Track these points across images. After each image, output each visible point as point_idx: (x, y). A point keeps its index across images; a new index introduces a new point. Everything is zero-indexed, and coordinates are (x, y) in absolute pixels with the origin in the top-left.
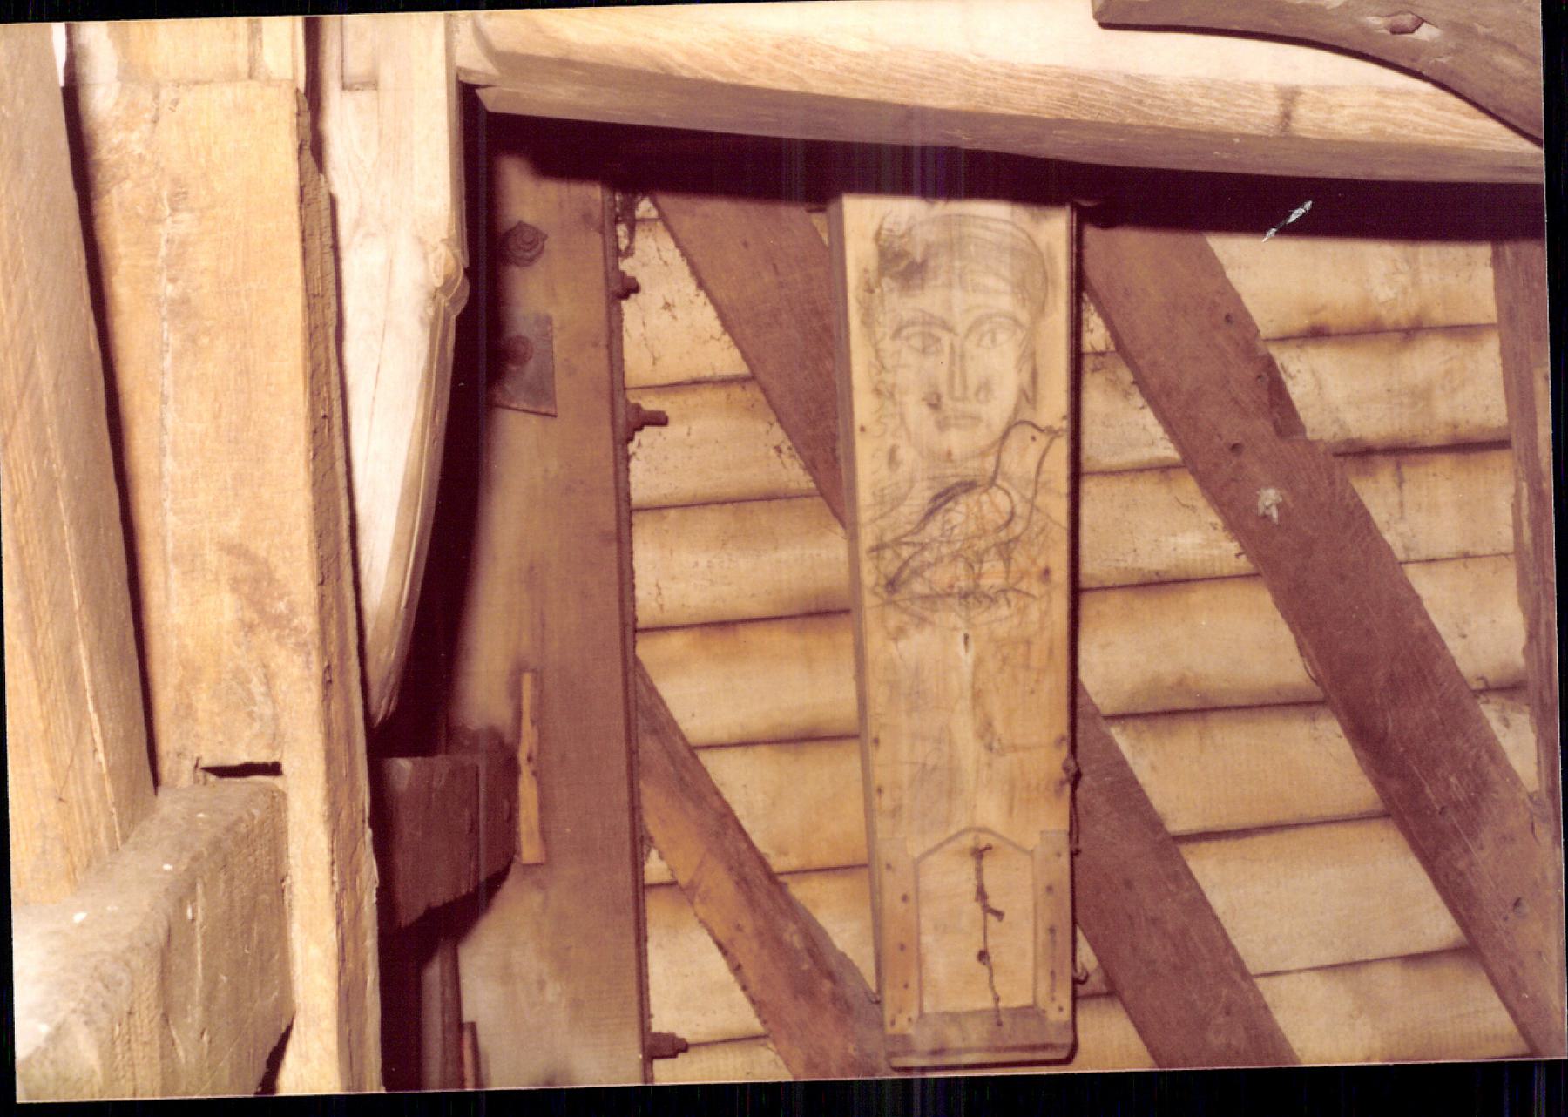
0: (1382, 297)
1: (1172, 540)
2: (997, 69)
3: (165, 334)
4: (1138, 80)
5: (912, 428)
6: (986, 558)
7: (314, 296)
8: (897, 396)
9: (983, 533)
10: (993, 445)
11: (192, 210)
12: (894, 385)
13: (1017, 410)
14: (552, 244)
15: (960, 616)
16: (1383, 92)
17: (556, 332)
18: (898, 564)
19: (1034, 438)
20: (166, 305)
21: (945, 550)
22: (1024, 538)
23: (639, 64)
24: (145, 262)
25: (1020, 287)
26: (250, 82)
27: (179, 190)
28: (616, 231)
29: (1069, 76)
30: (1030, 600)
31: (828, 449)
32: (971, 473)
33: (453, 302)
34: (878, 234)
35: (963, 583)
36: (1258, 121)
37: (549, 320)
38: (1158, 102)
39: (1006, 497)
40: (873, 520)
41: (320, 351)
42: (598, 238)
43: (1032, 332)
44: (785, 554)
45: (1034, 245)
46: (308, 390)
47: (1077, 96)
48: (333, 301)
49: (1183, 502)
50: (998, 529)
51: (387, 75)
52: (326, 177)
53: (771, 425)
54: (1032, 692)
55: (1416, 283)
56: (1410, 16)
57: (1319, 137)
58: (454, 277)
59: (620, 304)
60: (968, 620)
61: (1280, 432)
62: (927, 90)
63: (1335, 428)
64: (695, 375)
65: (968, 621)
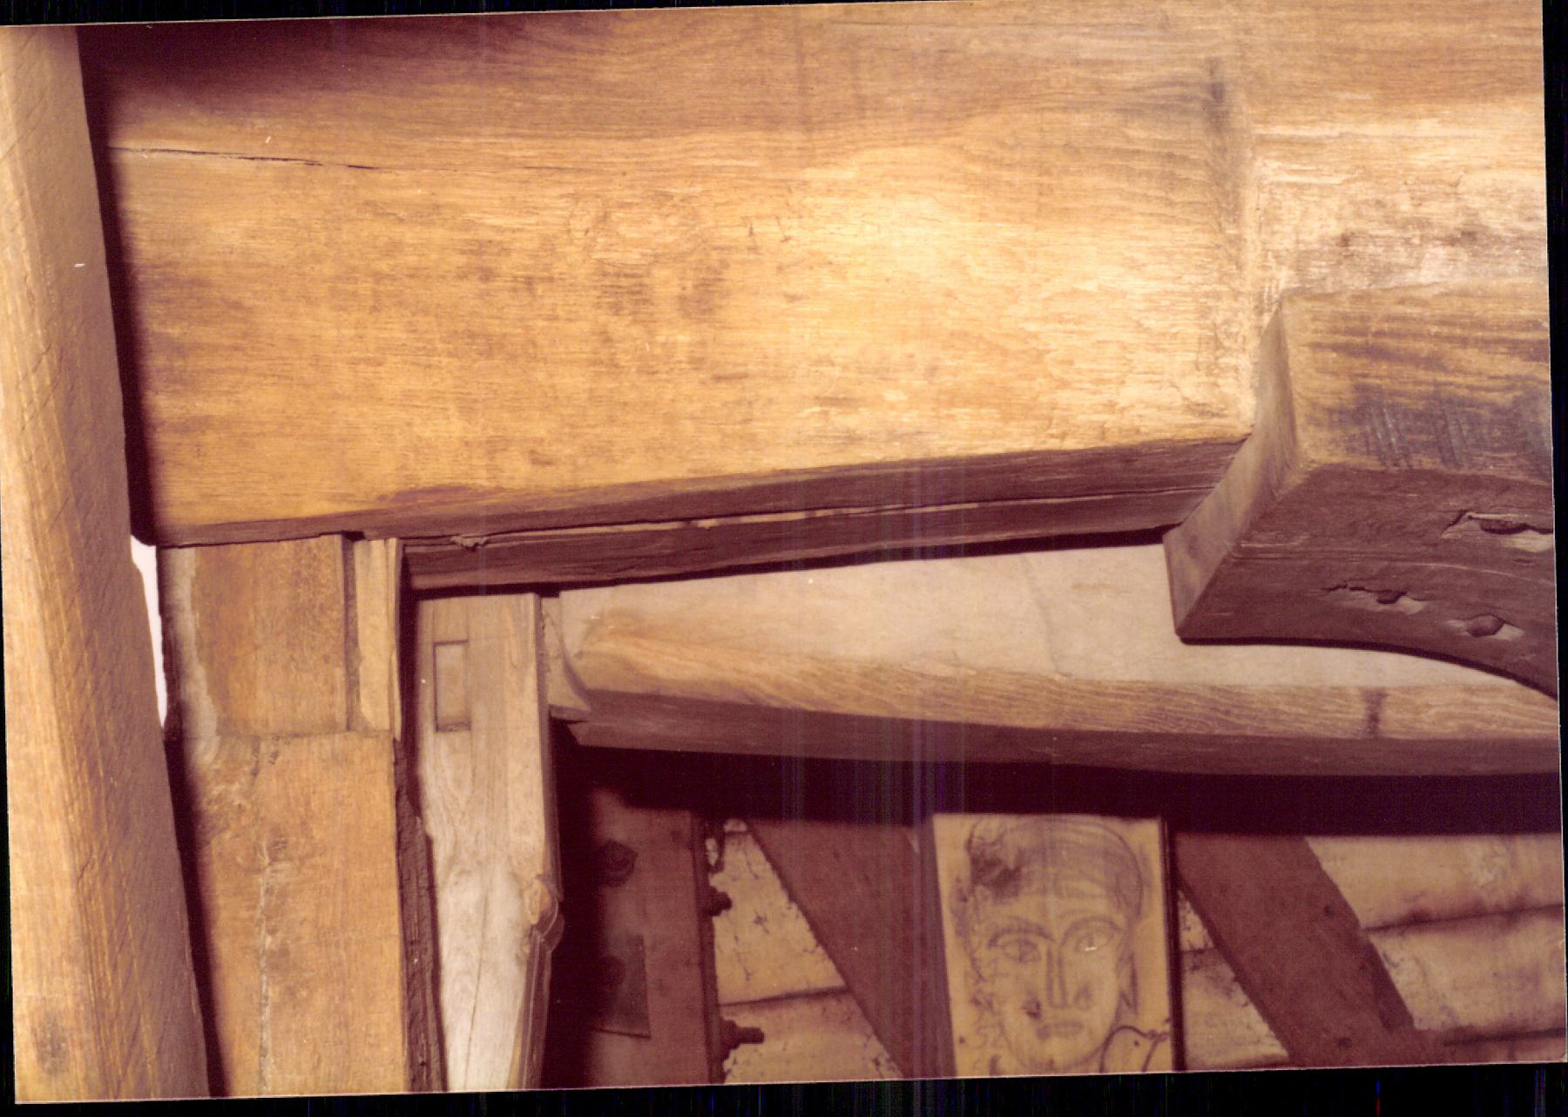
0: (1482, 881)
2: (1083, 687)
3: (264, 987)
4: (1226, 691)
7: (412, 943)
8: (996, 1005)
10: (1093, 1055)
11: (290, 859)
12: (992, 995)
13: (1118, 1014)
14: (641, 863)
16: (1469, 690)
17: (648, 953)
20: (265, 958)
23: (730, 697)
24: (244, 914)
25: (1116, 891)
26: (347, 734)
27: (278, 839)
29: (1154, 690)
33: (548, 939)
34: (970, 841)
36: (1347, 725)
37: (640, 940)
38: (1246, 712)
41: (418, 998)
42: (685, 855)
45: (1126, 847)
46: (406, 1040)
47: (1164, 710)
48: (429, 946)
51: (480, 714)
52: (422, 818)
55: (1514, 865)
56: (1491, 618)
57: (1409, 737)
58: (550, 913)
59: (711, 920)
61: (1388, 1025)
62: (1015, 710)
63: (1444, 1017)
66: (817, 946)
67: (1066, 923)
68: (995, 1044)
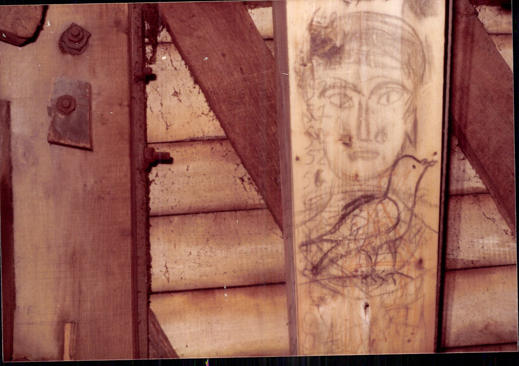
1: (481, 241)
5: (332, 159)
6: (380, 252)
8: (322, 137)
9: (378, 233)
10: (387, 170)
12: (320, 129)
13: (403, 148)
14: (94, 41)
15: (362, 290)
18: (320, 255)
19: (414, 167)
21: (352, 246)
22: (406, 237)
28: (145, 47)
30: (409, 280)
31: (273, 178)
32: (371, 188)
35: (365, 269)
39: (394, 207)
40: (304, 223)
43: (414, 93)
44: (245, 248)
49: (488, 216)
50: (388, 231)
53: (238, 165)
54: (409, 341)
60: (367, 293)
64: (192, 136)
65: (367, 294)
66: (210, 111)
67: (373, 84)
68: (319, 163)
